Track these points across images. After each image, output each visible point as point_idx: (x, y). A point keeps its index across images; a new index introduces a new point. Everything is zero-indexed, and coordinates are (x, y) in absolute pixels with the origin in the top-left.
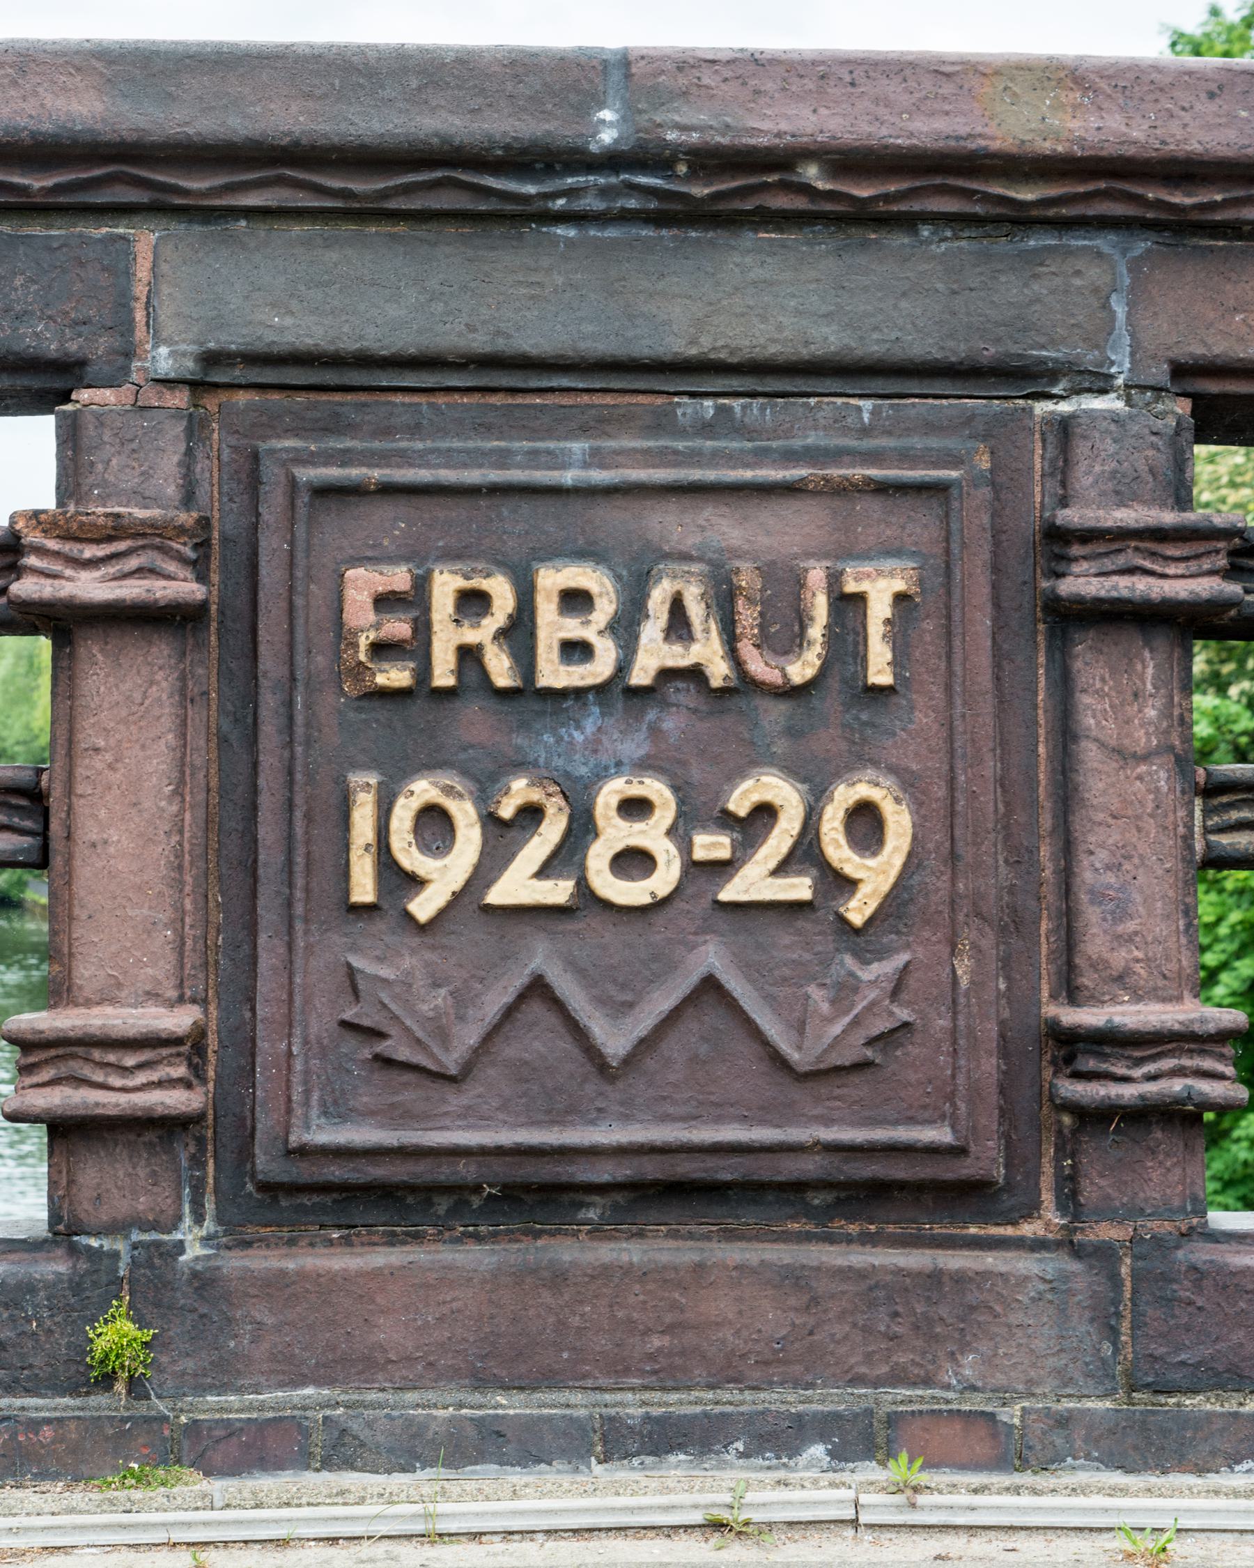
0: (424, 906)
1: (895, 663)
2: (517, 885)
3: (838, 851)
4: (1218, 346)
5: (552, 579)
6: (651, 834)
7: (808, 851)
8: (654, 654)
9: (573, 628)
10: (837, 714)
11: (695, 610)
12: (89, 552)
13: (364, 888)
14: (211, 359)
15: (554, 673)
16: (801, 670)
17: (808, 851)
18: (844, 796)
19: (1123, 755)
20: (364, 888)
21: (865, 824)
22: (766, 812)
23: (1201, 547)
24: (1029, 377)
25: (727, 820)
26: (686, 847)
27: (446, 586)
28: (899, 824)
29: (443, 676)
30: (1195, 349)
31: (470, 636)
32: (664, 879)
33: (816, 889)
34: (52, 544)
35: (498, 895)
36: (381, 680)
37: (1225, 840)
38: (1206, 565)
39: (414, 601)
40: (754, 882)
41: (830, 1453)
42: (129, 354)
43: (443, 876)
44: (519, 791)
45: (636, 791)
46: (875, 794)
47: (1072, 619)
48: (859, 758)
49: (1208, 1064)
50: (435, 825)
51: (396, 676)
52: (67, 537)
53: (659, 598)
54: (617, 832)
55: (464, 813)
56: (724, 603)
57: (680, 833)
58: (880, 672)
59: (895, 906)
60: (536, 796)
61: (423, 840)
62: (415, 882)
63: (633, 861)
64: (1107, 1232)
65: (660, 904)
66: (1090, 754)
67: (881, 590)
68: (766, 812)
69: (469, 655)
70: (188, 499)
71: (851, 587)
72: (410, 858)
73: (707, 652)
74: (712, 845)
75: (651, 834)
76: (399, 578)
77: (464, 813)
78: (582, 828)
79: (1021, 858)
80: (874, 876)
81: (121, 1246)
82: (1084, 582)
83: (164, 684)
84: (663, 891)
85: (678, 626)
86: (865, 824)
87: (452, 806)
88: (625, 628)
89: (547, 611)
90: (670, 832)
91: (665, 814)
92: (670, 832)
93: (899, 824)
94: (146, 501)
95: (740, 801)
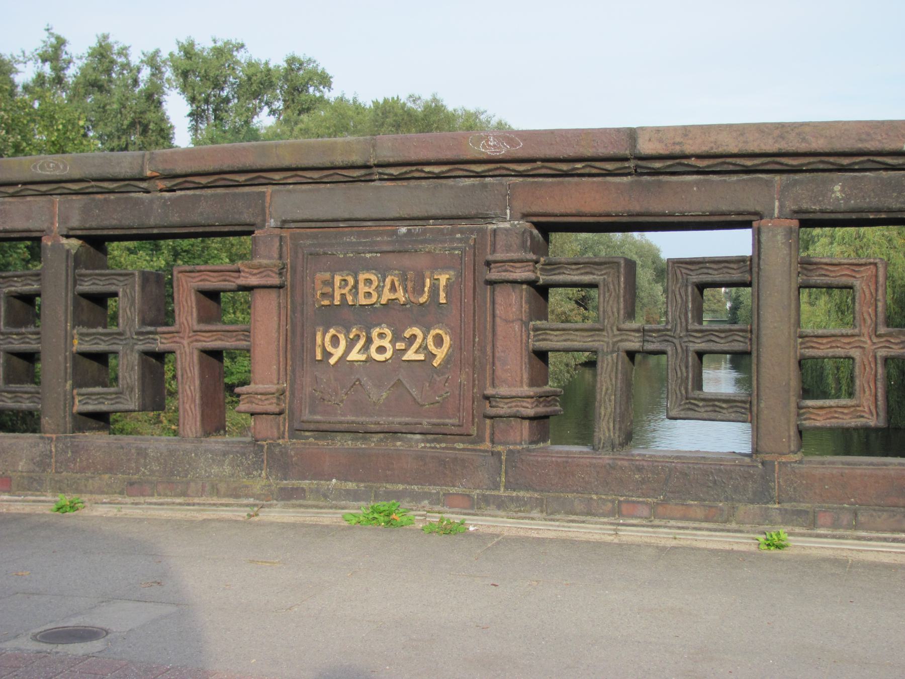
0: (332, 361)
1: (446, 297)
2: (354, 356)
3: (432, 347)
4: (535, 209)
5: (362, 277)
6: (386, 343)
7: (423, 348)
8: (387, 296)
9: (367, 289)
10: (425, 314)
11: (397, 284)
12: (255, 271)
13: (319, 357)
14: (284, 222)
15: (363, 301)
16: (422, 300)
17: (423, 348)
18: (433, 332)
19: (507, 321)
20: (319, 357)
21: (439, 341)
22: (414, 337)
23: (525, 264)
24: (486, 218)
25: (403, 339)
26: (394, 346)
27: (338, 279)
28: (447, 340)
29: (337, 302)
30: (526, 210)
31: (343, 292)
32: (388, 354)
33: (425, 357)
34: (246, 270)
35: (349, 358)
36: (323, 303)
37: (537, 343)
38: (527, 268)
39: (331, 283)
40: (410, 355)
41: (430, 503)
42: (264, 221)
43: (337, 353)
44: (354, 331)
45: (382, 331)
46: (440, 332)
47: (492, 283)
48: (438, 322)
49: (525, 404)
50: (335, 341)
51: (326, 302)
52: (250, 268)
53: (388, 280)
54: (377, 342)
55: (342, 337)
56: (404, 280)
57: (393, 342)
58: (443, 300)
59: (447, 360)
60: (358, 333)
61: (336, 347)
62: (330, 355)
63: (381, 350)
64: (500, 448)
65: (387, 360)
66: (498, 320)
67: (443, 279)
68: (414, 337)
69: (343, 295)
70: (280, 258)
71: (436, 277)
72: (329, 349)
73: (401, 296)
74: (400, 345)
75: (386, 343)
76: (327, 275)
77: (342, 337)
78: (369, 341)
79: (483, 351)
80: (441, 354)
81: (264, 443)
82: (494, 275)
83: (275, 304)
84: (388, 357)
85: (393, 288)
86: (439, 341)
87: (339, 335)
88: (379, 290)
89: (361, 285)
90: (390, 342)
91: (389, 337)
92: (390, 342)
93: (447, 340)
94: (270, 258)
95: (407, 334)
